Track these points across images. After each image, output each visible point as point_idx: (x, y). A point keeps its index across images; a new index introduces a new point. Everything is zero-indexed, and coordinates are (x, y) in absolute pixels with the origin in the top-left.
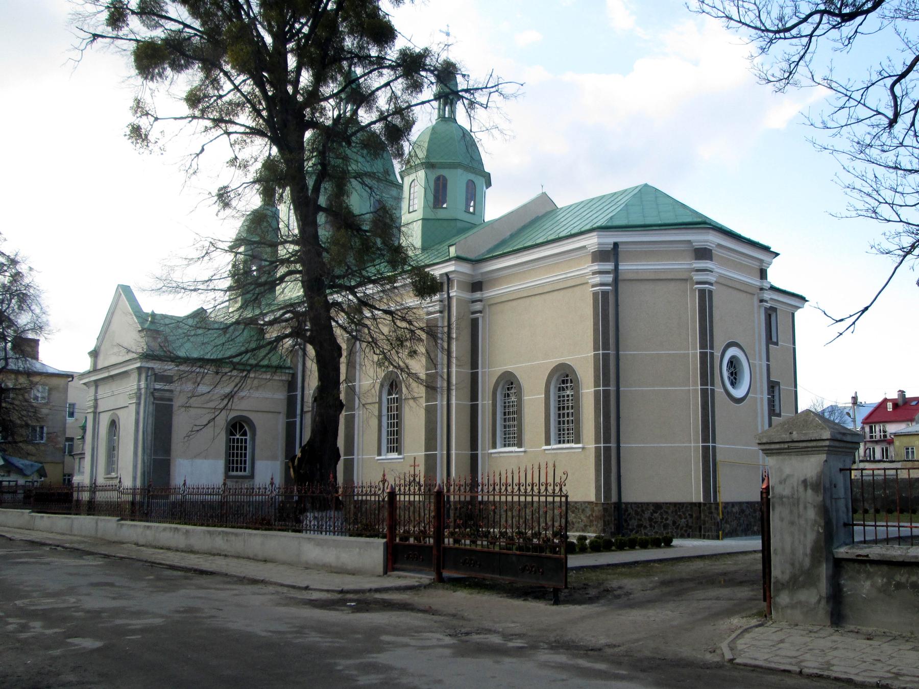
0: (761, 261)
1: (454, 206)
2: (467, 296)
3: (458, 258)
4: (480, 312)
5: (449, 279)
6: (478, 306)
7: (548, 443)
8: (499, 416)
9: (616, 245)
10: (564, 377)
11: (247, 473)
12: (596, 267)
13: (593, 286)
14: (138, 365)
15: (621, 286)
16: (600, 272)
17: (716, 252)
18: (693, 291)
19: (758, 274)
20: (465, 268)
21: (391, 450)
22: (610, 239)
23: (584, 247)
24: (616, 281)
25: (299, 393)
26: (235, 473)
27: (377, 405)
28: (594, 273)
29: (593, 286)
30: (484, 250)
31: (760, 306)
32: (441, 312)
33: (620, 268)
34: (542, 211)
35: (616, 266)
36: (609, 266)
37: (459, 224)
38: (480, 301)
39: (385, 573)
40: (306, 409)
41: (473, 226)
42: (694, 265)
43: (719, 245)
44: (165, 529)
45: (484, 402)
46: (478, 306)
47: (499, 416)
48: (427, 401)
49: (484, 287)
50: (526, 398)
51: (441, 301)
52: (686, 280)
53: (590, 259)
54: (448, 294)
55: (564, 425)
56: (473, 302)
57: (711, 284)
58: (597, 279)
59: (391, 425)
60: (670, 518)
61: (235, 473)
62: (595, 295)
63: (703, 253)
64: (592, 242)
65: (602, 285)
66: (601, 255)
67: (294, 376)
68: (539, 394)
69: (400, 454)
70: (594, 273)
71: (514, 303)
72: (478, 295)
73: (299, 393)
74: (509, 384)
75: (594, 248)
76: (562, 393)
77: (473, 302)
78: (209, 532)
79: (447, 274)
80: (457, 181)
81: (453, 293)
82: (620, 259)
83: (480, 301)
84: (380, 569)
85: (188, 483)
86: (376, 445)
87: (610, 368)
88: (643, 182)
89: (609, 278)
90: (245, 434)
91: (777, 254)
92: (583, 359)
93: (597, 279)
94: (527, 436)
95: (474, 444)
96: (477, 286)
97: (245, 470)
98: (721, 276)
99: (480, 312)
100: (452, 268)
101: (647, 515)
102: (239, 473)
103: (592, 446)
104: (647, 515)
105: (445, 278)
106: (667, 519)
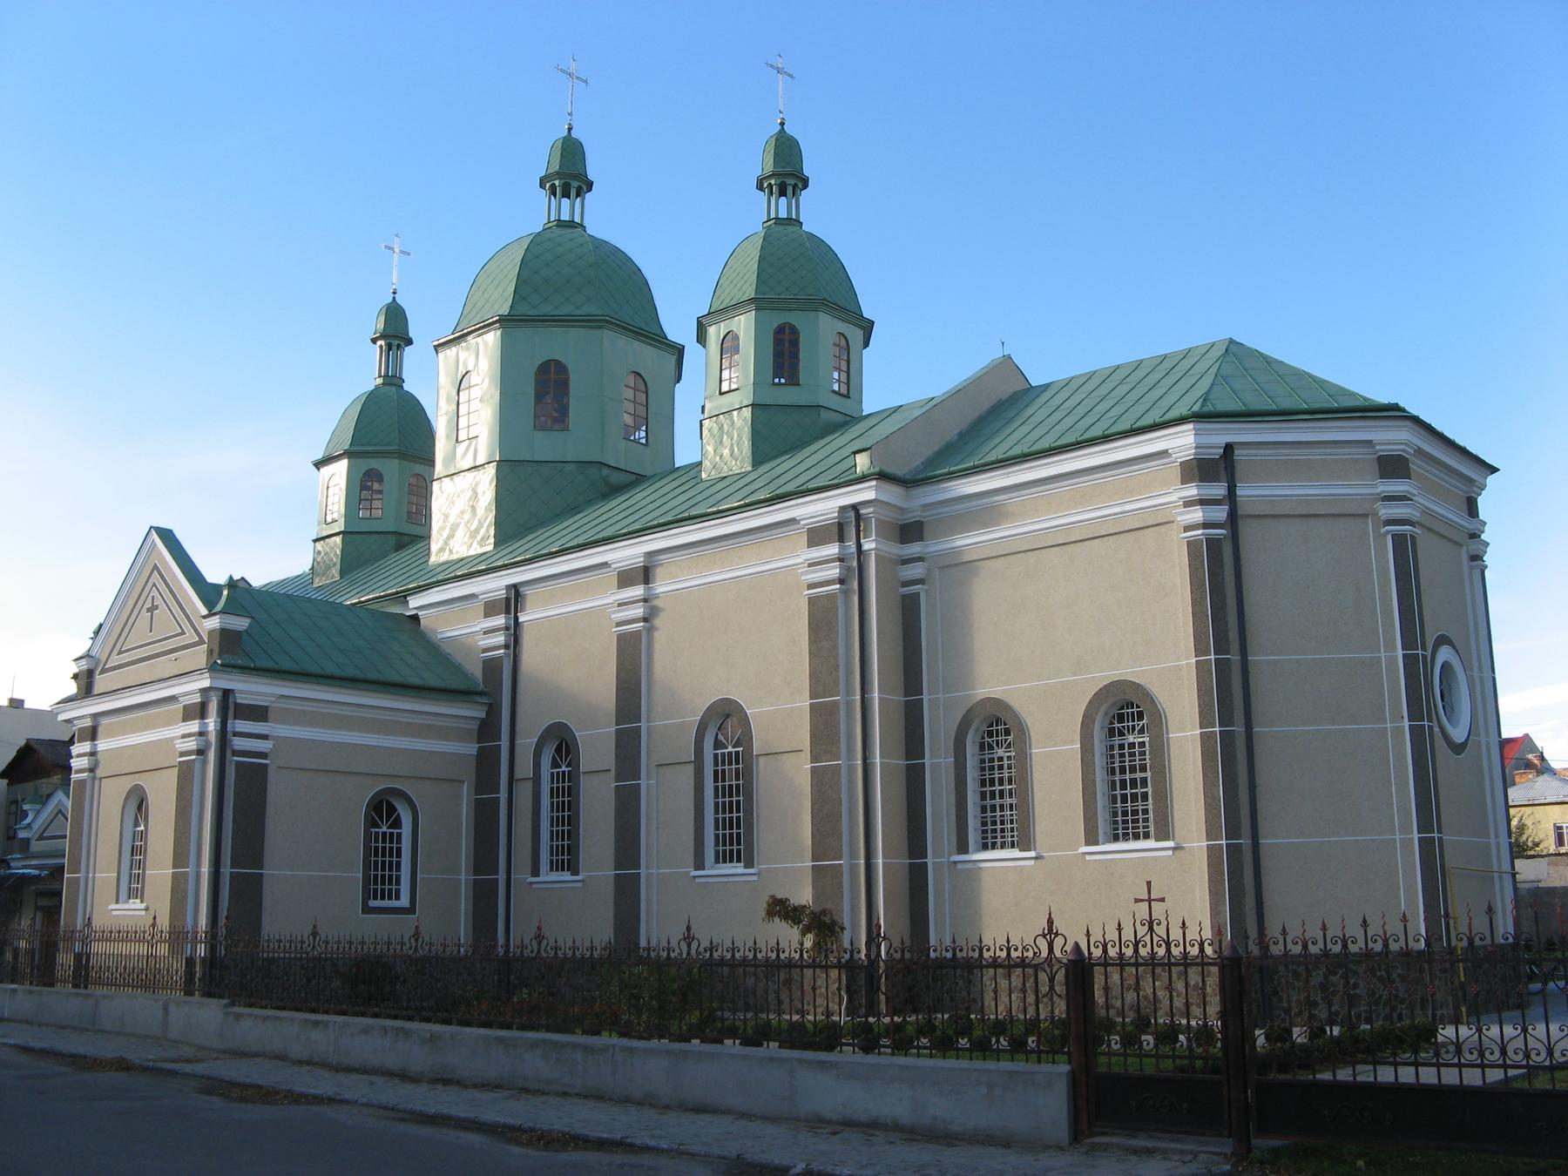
0: (1471, 481)
1: (820, 378)
2: (895, 549)
3: (882, 476)
4: (920, 581)
5: (858, 517)
6: (916, 571)
7: (1091, 839)
8: (972, 786)
9: (1229, 448)
10: (1123, 714)
11: (404, 901)
12: (1192, 491)
13: (1187, 528)
14: (206, 683)
15: (1246, 529)
16: (1203, 502)
17: (1416, 465)
18: (1380, 538)
19: (1465, 506)
20: (892, 494)
21: (724, 857)
22: (1220, 436)
23: (1164, 453)
24: (1233, 515)
25: (504, 743)
26: (378, 903)
27: (691, 769)
28: (1188, 504)
29: (1187, 528)
30: (918, 461)
31: (1471, 568)
32: (841, 581)
33: (1239, 492)
34: (1006, 391)
35: (1232, 489)
36: (1219, 490)
37: (825, 415)
38: (920, 559)
39: (1077, 1135)
40: (518, 775)
41: (851, 420)
42: (1381, 488)
43: (1419, 452)
44: (366, 1031)
45: (937, 761)
46: (916, 571)
47: (972, 786)
48: (814, 758)
49: (926, 533)
50: (1037, 751)
51: (841, 560)
52: (1365, 516)
53: (1176, 473)
54: (859, 546)
55: (1126, 797)
56: (905, 562)
57: (1412, 524)
58: (1197, 515)
59: (560, 807)
60: (1362, 984)
61: (378, 903)
62: (1192, 546)
63: (1393, 466)
64: (1182, 442)
65: (1205, 525)
66: (1201, 469)
67: (493, 710)
68: (1072, 742)
69: (749, 864)
70: (1188, 504)
71: (999, 563)
72: (914, 549)
73: (504, 743)
74: (997, 727)
75: (1189, 454)
76: (1117, 740)
77: (905, 562)
78: (500, 1040)
79: (855, 507)
80: (821, 332)
81: (868, 545)
82: (1237, 474)
83: (920, 559)
84: (1062, 1132)
85: (322, 932)
86: (691, 843)
87: (1231, 689)
88: (1222, 335)
89: (1221, 513)
90: (397, 824)
91: (1494, 470)
92: (1172, 669)
93: (1197, 515)
94: (1043, 826)
95: (916, 842)
96: (909, 531)
97: (398, 898)
98: (1426, 512)
99: (920, 581)
100: (870, 495)
101: (1317, 978)
102: (386, 903)
103: (1198, 844)
104: (1317, 978)
105: (852, 514)
106: (1356, 986)
